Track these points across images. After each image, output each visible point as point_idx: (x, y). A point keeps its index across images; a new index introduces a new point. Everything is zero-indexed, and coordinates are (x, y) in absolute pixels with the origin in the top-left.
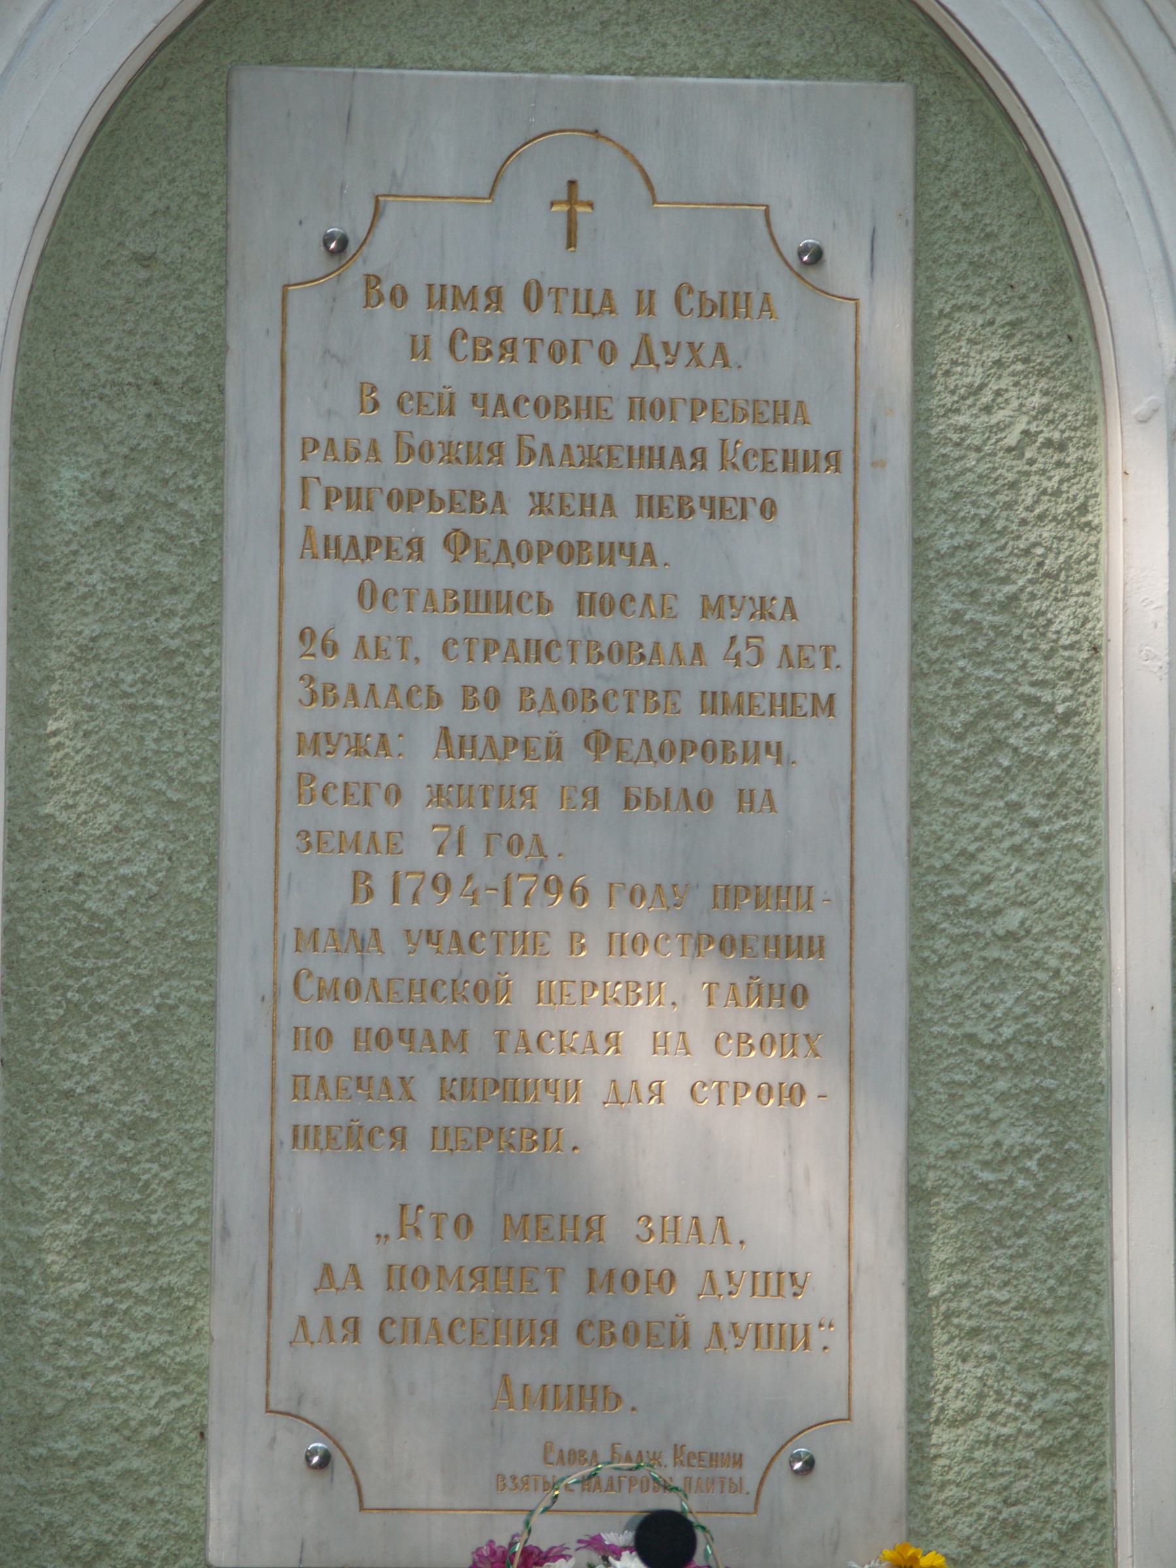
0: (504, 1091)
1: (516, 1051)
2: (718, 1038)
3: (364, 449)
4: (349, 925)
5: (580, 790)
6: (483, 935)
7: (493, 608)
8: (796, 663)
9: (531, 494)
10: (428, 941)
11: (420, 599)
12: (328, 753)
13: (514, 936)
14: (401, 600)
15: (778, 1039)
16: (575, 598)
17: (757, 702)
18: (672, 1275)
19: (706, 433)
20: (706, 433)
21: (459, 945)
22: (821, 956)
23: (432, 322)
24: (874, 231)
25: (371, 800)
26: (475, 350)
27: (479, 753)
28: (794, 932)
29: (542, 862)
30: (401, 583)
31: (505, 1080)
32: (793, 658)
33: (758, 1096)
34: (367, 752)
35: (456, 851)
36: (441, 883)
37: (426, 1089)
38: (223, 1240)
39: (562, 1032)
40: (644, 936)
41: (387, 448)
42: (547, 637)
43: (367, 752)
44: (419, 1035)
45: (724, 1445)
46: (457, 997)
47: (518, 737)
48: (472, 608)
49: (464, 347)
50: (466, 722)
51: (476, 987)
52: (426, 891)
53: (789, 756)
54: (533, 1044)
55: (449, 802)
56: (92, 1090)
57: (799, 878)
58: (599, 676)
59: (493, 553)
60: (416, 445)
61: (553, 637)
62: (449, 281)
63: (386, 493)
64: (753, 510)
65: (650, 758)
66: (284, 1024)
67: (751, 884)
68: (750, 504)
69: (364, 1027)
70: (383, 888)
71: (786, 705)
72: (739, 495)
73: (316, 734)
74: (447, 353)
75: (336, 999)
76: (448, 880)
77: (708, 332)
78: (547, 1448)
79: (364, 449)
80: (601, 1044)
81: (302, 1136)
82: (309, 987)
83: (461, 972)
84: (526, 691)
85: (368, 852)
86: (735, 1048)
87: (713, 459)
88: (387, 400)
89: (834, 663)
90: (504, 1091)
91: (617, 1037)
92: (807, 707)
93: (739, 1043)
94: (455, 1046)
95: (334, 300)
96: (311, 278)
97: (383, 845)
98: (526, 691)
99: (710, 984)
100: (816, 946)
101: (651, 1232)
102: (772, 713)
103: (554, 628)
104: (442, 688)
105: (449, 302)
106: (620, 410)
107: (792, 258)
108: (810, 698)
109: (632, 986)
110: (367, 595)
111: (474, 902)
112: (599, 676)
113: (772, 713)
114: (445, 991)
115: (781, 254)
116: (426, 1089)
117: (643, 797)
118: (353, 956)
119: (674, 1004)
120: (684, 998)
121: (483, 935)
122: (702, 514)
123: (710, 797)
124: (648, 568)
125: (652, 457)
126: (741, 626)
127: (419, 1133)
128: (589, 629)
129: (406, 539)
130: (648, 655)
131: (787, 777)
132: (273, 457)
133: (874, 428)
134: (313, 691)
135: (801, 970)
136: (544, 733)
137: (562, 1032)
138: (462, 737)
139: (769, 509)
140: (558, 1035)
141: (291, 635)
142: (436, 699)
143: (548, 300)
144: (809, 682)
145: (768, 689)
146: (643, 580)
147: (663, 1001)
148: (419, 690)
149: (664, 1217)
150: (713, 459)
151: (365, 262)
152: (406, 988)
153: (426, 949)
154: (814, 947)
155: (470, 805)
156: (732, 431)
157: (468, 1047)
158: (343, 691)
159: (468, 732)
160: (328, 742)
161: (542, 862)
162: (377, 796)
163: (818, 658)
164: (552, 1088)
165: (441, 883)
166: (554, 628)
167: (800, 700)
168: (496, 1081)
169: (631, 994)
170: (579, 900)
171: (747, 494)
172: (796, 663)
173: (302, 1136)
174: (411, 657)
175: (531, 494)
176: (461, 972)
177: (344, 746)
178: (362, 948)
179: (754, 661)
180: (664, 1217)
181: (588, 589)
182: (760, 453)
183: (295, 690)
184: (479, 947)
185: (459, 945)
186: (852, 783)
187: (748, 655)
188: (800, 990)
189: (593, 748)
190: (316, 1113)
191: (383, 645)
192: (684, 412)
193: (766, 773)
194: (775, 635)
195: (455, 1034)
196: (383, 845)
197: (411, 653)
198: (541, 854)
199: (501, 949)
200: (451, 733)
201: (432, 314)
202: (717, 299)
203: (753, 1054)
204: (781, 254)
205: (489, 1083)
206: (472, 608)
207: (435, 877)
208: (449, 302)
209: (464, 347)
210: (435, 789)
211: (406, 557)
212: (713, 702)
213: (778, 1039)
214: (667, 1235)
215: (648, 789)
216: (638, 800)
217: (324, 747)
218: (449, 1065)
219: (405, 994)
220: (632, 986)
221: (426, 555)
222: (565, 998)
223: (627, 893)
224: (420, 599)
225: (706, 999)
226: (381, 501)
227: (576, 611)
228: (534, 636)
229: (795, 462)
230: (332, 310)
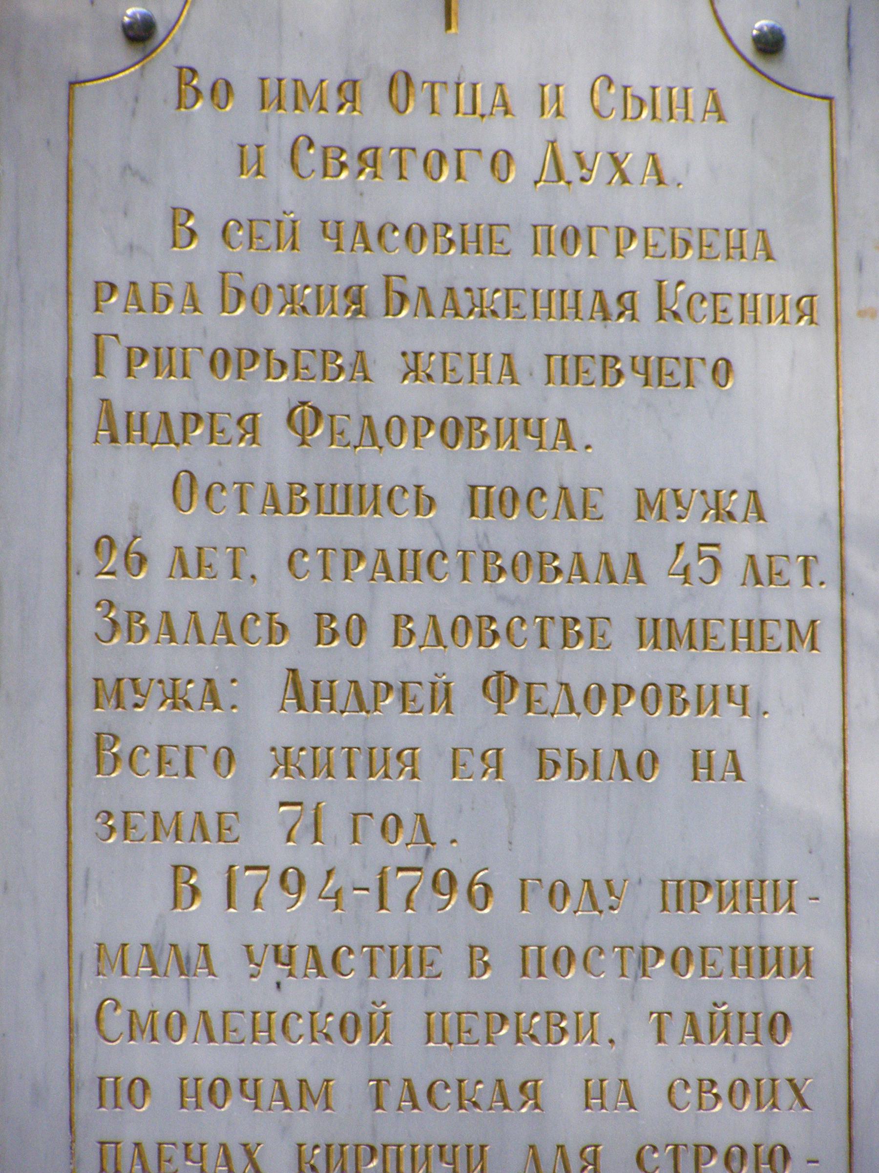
0: (384, 1161)
1: (399, 1109)
2: (671, 1087)
3: (177, 293)
4: (170, 939)
5: (479, 754)
6: (350, 951)
7: (354, 507)
8: (765, 578)
9: (404, 354)
10: (277, 960)
11: (256, 497)
12: (136, 705)
13: (392, 953)
14: (229, 497)
15: (753, 1086)
16: (464, 493)
17: (718, 631)
18: (228, 84)
21: (318, 965)
22: (807, 973)
23: (267, 128)
24: (849, 9)
25: (194, 768)
26: (325, 164)
27: (339, 704)
28: (772, 940)
29: (428, 850)
30: (230, 474)
31: (385, 1146)
33: (727, 1163)
34: (187, 704)
35: (312, 837)
36: (292, 880)
39: (461, 1081)
40: (569, 950)
41: (209, 296)
42: (428, 546)
43: (187, 704)
44: (267, 1089)
46: (317, 1035)
47: (391, 681)
48: (326, 507)
49: (311, 158)
51: (343, 1020)
52: (272, 892)
53: (759, 705)
54: (422, 1098)
55: (301, 772)
58: (502, 598)
59: (353, 435)
60: (247, 290)
61: (437, 546)
62: (289, 72)
63: (208, 355)
64: (703, 373)
65: (572, 709)
67: (712, 879)
68: (696, 364)
69: (192, 1076)
72: (682, 354)
73: (119, 680)
74: (287, 167)
75: (154, 1039)
76: (301, 878)
79: (177, 293)
80: (514, 1097)
82: (116, 1022)
83: (321, 1001)
84: (400, 620)
85: (192, 840)
86: (695, 1101)
87: (646, 306)
88: (209, 233)
89: (815, 579)
90: (384, 1161)
91: (535, 1087)
92: (782, 637)
93: (700, 1091)
94: (315, 1102)
95: (136, 99)
96: (106, 73)
97: (212, 829)
98: (400, 620)
99: (660, 1014)
100: (800, 960)
101: (112, 829)
102: (734, 647)
103: (437, 535)
104: (285, 615)
105: (288, 102)
106: (520, 243)
107: (748, 49)
108: (785, 625)
109: (555, 1017)
111: (337, 906)
112: (502, 598)
113: (734, 647)
114: (301, 1026)
115: (729, 39)
117: (563, 761)
118: (176, 981)
119: (611, 1041)
120: (625, 1033)
121: (350, 951)
122: (630, 383)
123: (655, 759)
124: (562, 454)
128: (486, 535)
129: (236, 416)
130: (566, 570)
131: (757, 734)
132: (54, 312)
134: (114, 622)
136: (426, 676)
137: (461, 1081)
138: (317, 682)
140: (456, 1084)
141: (83, 551)
145: (728, 616)
147: (596, 1038)
148: (257, 618)
149: (478, 225)
150: (646, 306)
151: (176, 50)
152: (247, 1020)
153: (273, 971)
155: (329, 774)
156: (670, 269)
157: (332, 1103)
158: (153, 620)
159: (323, 675)
160: (136, 691)
161: (428, 850)
162: (202, 762)
163: (795, 573)
164: (448, 1157)
165: (292, 880)
166: (437, 535)
167: (771, 628)
168: (372, 1149)
169: (553, 1029)
170: (480, 902)
171: (696, 352)
172: (765, 578)
174: (246, 576)
175: (404, 354)
176: (321, 1001)
177: (156, 695)
178: (184, 968)
179: (708, 577)
180: (478, 225)
181: (481, 479)
182: (710, 298)
184: (344, 967)
185: (318, 965)
186: (844, 739)
187: (701, 567)
188: (780, 1019)
189: (494, 696)
191: (206, 559)
192: (605, 243)
195: (315, 1085)
196: (212, 829)
197: (245, 570)
198: (427, 840)
199: (376, 970)
200: (301, 676)
201: (267, 117)
202: (647, 96)
203: (719, 1107)
204: (729, 39)
205: (364, 1151)
206: (326, 507)
207: (284, 874)
208: (288, 102)
209: (311, 158)
210: (281, 752)
211: (236, 439)
213: (753, 1086)
214: (676, 111)
215: (570, 751)
216: (557, 765)
217: (130, 697)
219: (247, 1031)
220: (555, 1017)
221: (262, 436)
222: (464, 1036)
223: (545, 892)
224: (256, 497)
225: (655, 1034)
226: (199, 364)
227: (468, 512)
228: (411, 544)
230: (133, 113)
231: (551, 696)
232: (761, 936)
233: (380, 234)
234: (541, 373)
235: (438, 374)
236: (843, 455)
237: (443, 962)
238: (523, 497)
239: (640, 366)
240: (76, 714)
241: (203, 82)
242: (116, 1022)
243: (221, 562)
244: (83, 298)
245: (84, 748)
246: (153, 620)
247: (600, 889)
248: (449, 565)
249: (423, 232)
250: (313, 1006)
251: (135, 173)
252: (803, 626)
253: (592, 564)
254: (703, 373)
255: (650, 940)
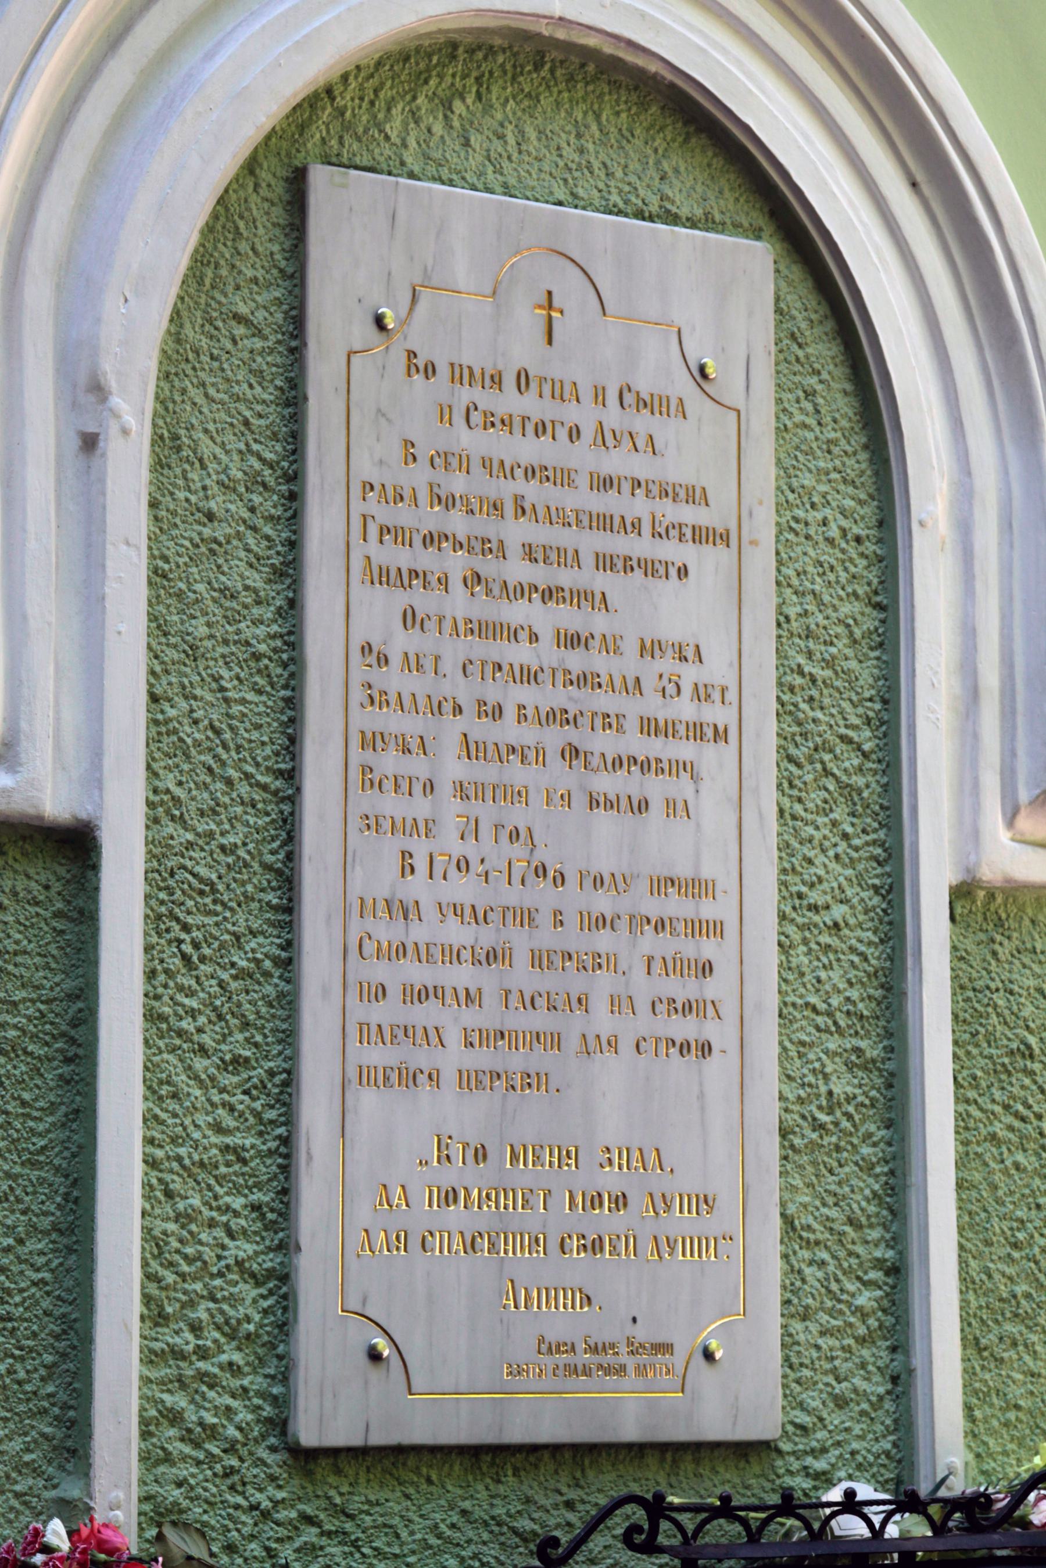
11: (448, 625)
19: (639, 507)
20: (639, 507)
32: (702, 694)
37: (453, 1037)
38: (308, 1164)
45: (660, 1339)
50: (482, 730)
56: (200, 1030)
57: (706, 873)
58: (570, 699)
64: (673, 572)
66: (351, 978)
70: (421, 864)
71: (697, 731)
77: (642, 423)
78: (541, 1340)
81: (366, 1076)
103: (538, 656)
110: (410, 618)
114: (466, 954)
116: (453, 1037)
120: (630, 968)
122: (638, 573)
125: (604, 523)
126: (667, 664)
127: (449, 1076)
132: (340, 497)
133: (751, 514)
135: (709, 948)
139: (683, 572)
142: (458, 710)
143: (534, 385)
144: (716, 714)
146: (599, 623)
151: (405, 338)
154: (716, 928)
163: (716, 696)
166: (538, 656)
173: (366, 1076)
176: (476, 940)
183: (358, 695)
187: (671, 689)
190: (377, 1056)
192: (626, 487)
193: (682, 787)
194: (689, 674)
197: (441, 672)
212: (650, 727)
218: (471, 1017)
228: (526, 661)
229: (701, 535)
231: (595, 761)
232: (697, 913)
233: (512, 469)
234: (593, 563)
235: (541, 558)
236: (737, 1114)
237: (539, 918)
238: (583, 640)
239: (643, 565)
240: (351, 753)
241: (420, 362)
242: (370, 948)
243: (428, 664)
244: (356, 491)
245: (355, 774)
246: (393, 698)
247: (619, 879)
248: (545, 677)
249: (534, 472)
250: (472, 942)
251: (383, 415)
252: (721, 729)
253: (618, 682)
254: (673, 572)
255: (644, 912)
